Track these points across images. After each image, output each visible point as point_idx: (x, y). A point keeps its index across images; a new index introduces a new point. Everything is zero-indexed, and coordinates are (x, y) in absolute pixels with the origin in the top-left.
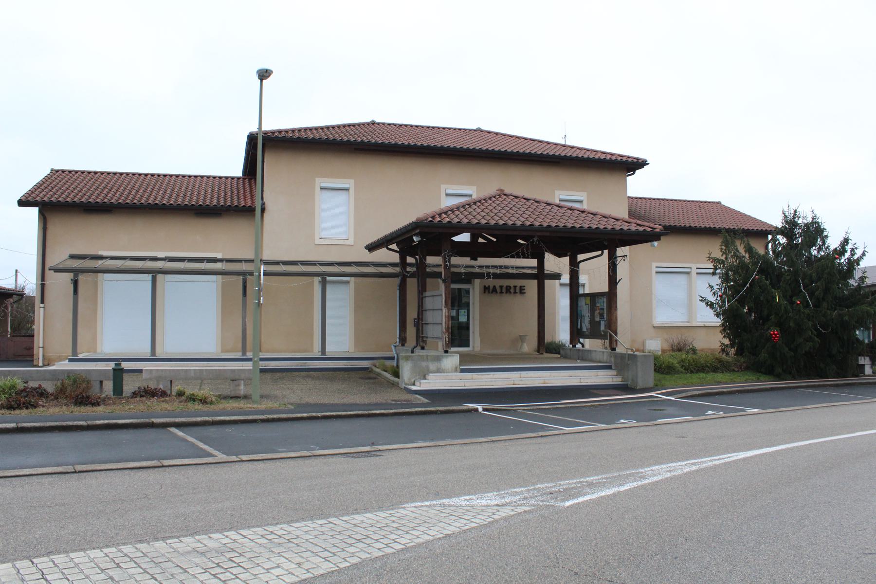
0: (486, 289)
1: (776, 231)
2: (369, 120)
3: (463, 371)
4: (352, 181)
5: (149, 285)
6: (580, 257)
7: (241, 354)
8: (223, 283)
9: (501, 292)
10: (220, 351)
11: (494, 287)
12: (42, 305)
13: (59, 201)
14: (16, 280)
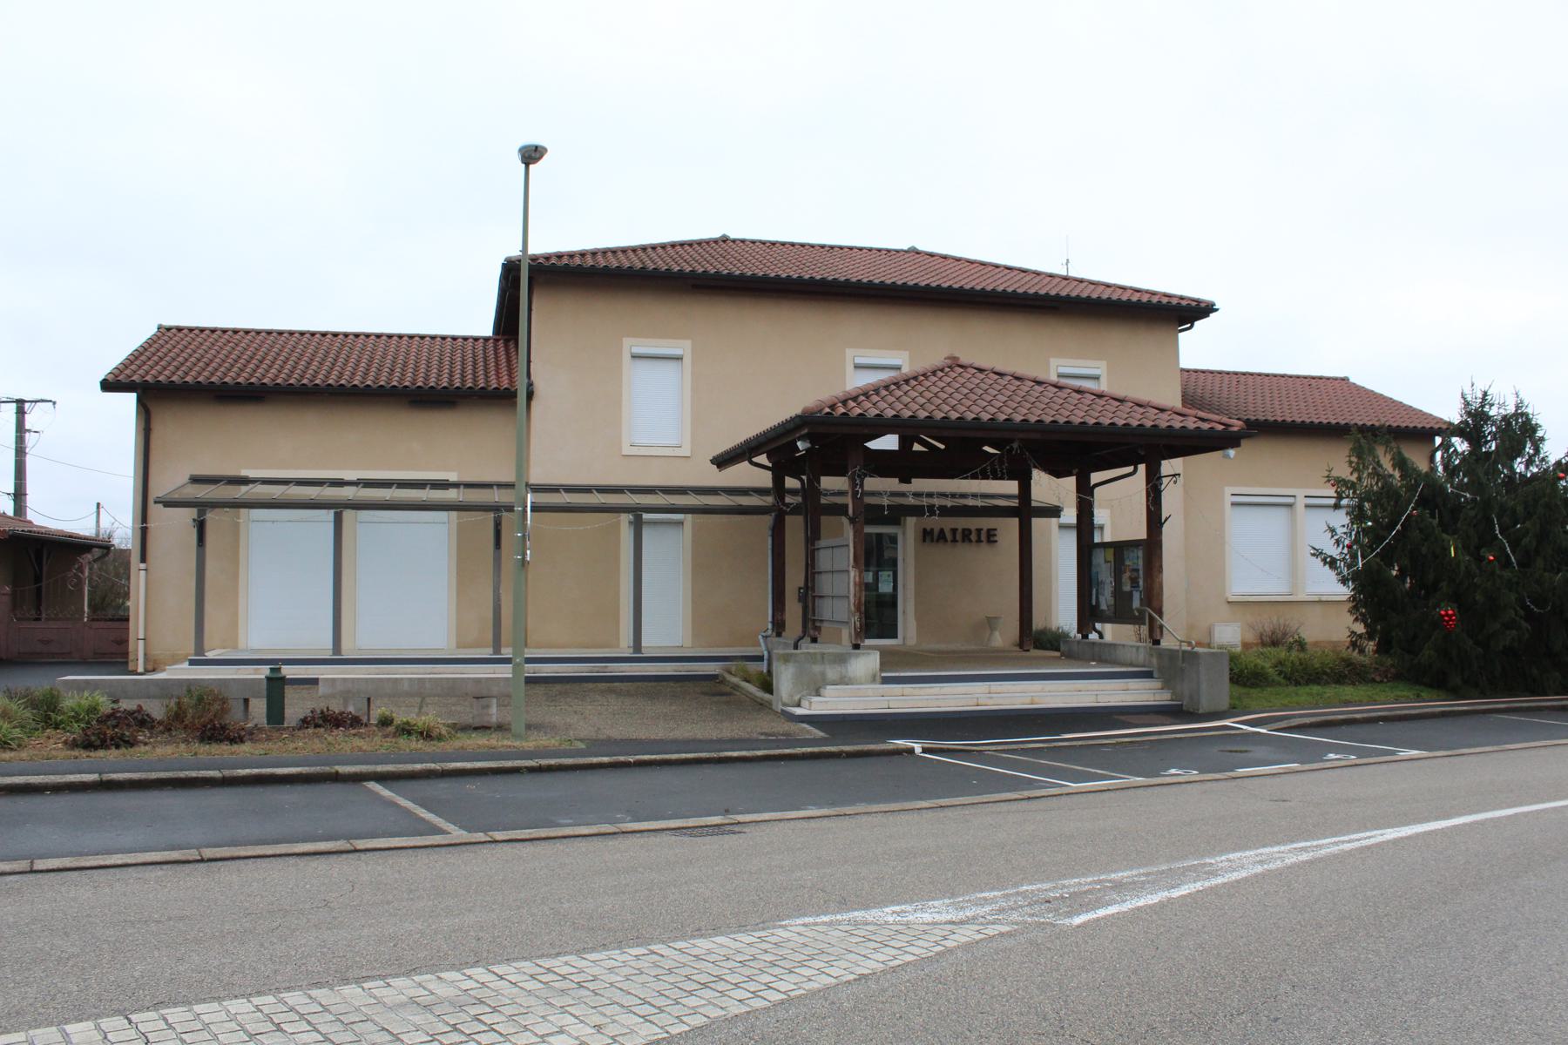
0: (926, 535)
1: (1449, 430)
3: (886, 681)
4: (688, 344)
5: (330, 528)
7: (491, 650)
8: (461, 529)
9: (954, 540)
11: (942, 531)
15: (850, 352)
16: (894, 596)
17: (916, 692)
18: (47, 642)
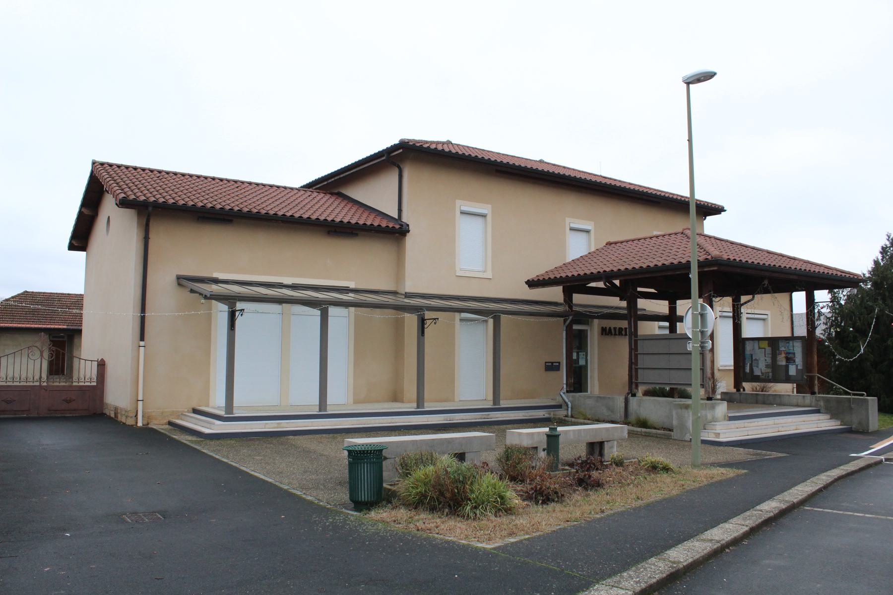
0: (605, 332)
1: (864, 281)
2: (396, 141)
3: (731, 419)
4: (490, 206)
5: (318, 320)
6: (744, 299)
7: (415, 405)
8: (357, 318)
9: (615, 334)
10: (351, 400)
12: (142, 343)
13: (128, 203)
14: (792, 310)
15: (568, 220)
16: (586, 367)
17: (749, 425)
18: (7, 402)
